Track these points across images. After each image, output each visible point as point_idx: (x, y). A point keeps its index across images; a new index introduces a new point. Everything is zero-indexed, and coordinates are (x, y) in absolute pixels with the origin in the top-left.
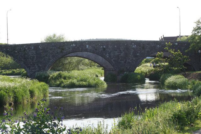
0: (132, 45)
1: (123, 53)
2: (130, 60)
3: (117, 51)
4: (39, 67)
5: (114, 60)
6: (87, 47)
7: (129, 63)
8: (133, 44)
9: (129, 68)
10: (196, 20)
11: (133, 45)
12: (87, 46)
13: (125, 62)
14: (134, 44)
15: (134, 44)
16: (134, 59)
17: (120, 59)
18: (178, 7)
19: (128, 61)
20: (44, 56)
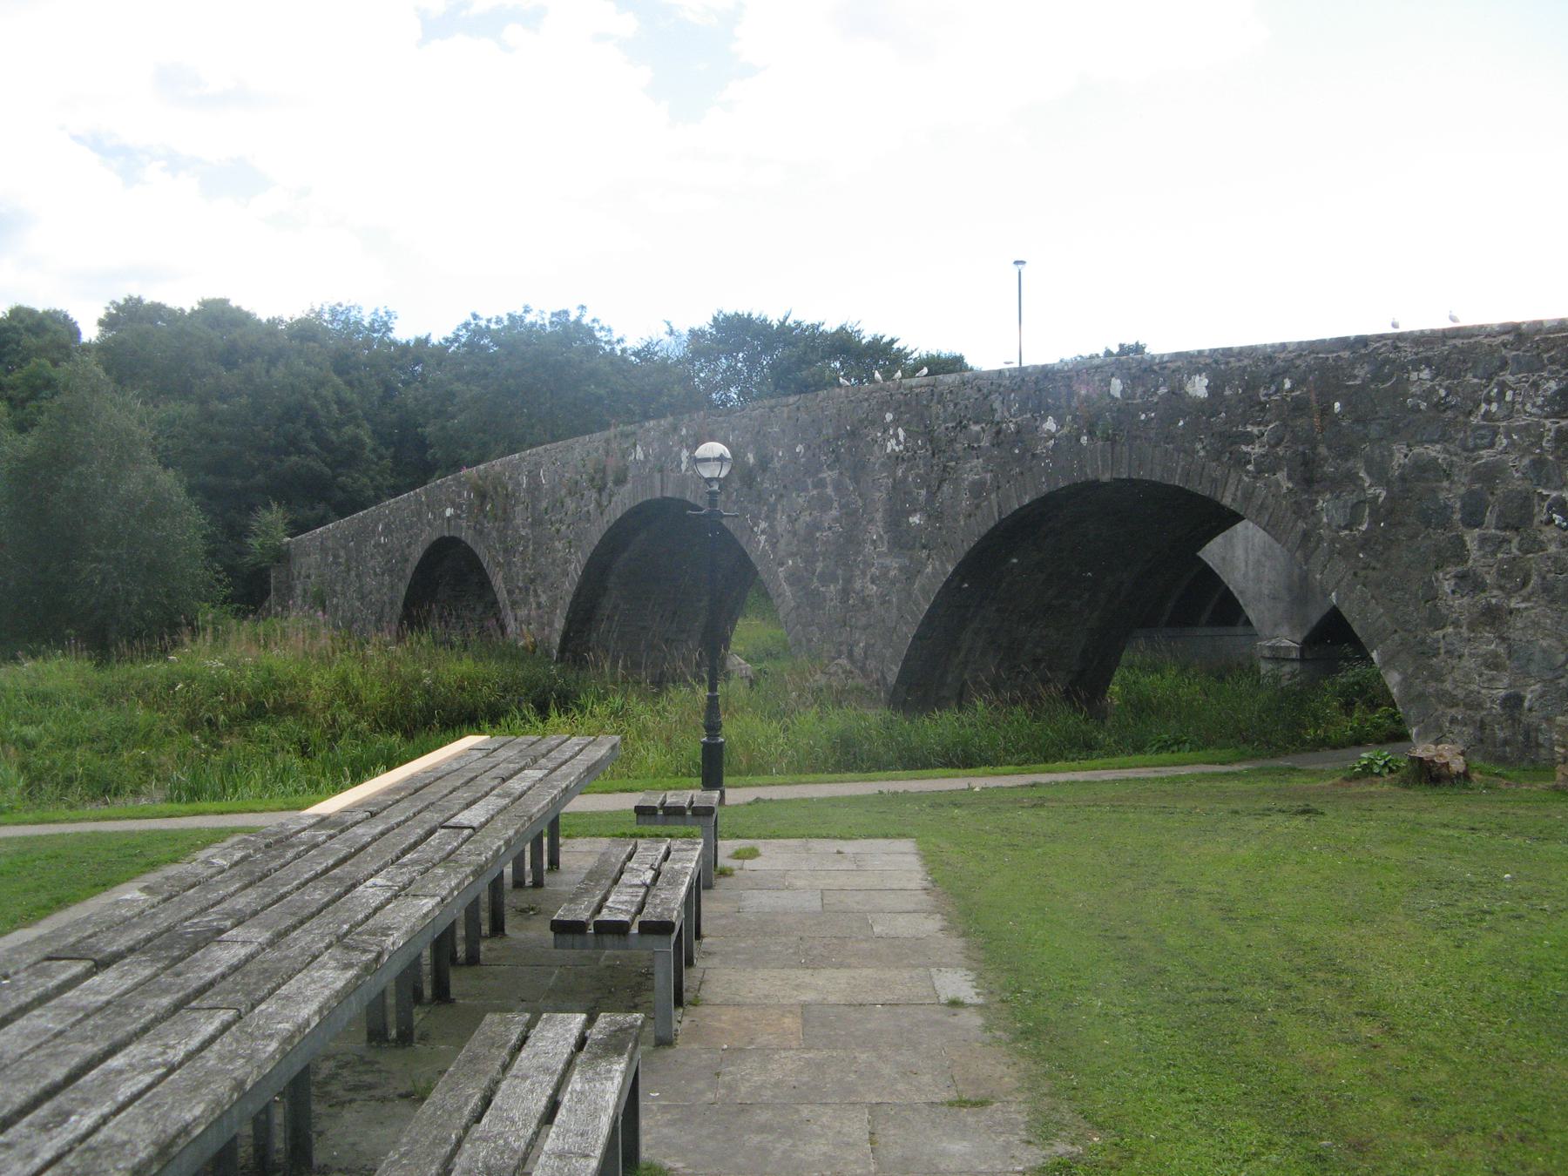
13: (845, 593)
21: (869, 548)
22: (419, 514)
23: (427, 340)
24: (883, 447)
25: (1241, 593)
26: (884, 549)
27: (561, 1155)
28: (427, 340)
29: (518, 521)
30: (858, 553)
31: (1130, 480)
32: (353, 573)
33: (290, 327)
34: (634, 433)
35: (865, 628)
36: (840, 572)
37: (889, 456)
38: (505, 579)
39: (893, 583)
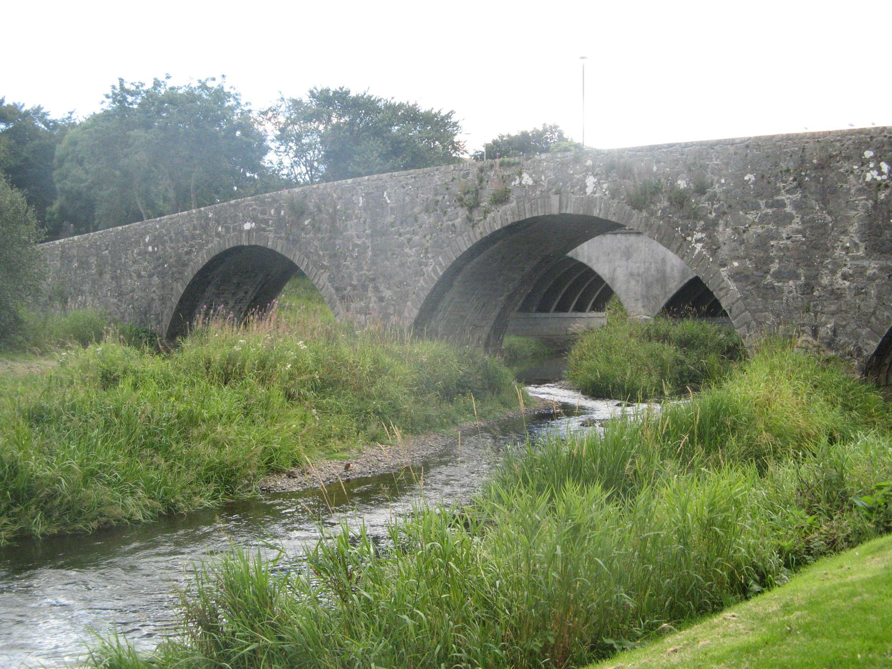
0: (864, 163)
1: (796, 224)
2: (845, 277)
3: (757, 207)
4: (381, 299)
5: (737, 276)
6: (589, 190)
7: (836, 294)
8: (868, 154)
9: (834, 332)
10: (557, 124)
11: (868, 161)
12: (590, 181)
13: (808, 288)
14: (878, 159)
15: (878, 159)
16: (872, 267)
17: (775, 267)
18: (223, 76)
19: (825, 281)
20: (401, 246)
21: (839, 252)
22: (205, 228)
23: (347, 93)
24: (860, 176)
25: (27, 590)
26: (861, 253)
27: (725, 619)
28: (347, 93)
29: (352, 232)
30: (825, 257)
31: (256, 246)
32: (107, 277)
33: (335, 93)
34: (519, 164)
35: (833, 314)
36: (801, 271)
37: (869, 184)
38: (331, 280)
39: (872, 279)
